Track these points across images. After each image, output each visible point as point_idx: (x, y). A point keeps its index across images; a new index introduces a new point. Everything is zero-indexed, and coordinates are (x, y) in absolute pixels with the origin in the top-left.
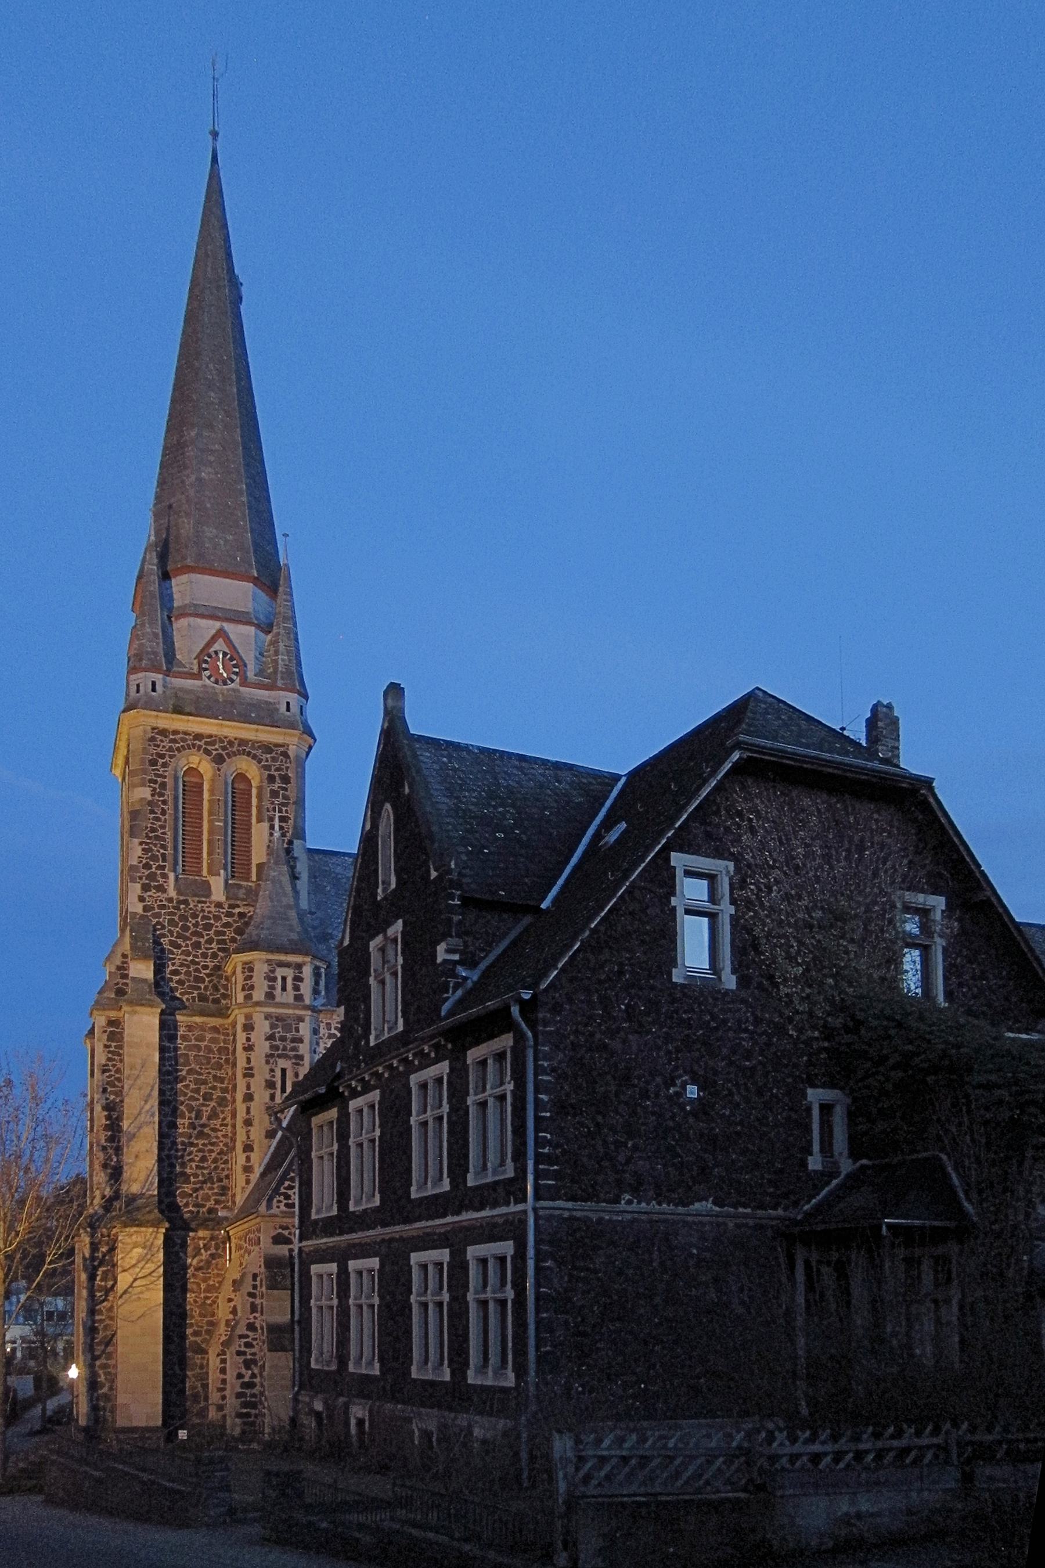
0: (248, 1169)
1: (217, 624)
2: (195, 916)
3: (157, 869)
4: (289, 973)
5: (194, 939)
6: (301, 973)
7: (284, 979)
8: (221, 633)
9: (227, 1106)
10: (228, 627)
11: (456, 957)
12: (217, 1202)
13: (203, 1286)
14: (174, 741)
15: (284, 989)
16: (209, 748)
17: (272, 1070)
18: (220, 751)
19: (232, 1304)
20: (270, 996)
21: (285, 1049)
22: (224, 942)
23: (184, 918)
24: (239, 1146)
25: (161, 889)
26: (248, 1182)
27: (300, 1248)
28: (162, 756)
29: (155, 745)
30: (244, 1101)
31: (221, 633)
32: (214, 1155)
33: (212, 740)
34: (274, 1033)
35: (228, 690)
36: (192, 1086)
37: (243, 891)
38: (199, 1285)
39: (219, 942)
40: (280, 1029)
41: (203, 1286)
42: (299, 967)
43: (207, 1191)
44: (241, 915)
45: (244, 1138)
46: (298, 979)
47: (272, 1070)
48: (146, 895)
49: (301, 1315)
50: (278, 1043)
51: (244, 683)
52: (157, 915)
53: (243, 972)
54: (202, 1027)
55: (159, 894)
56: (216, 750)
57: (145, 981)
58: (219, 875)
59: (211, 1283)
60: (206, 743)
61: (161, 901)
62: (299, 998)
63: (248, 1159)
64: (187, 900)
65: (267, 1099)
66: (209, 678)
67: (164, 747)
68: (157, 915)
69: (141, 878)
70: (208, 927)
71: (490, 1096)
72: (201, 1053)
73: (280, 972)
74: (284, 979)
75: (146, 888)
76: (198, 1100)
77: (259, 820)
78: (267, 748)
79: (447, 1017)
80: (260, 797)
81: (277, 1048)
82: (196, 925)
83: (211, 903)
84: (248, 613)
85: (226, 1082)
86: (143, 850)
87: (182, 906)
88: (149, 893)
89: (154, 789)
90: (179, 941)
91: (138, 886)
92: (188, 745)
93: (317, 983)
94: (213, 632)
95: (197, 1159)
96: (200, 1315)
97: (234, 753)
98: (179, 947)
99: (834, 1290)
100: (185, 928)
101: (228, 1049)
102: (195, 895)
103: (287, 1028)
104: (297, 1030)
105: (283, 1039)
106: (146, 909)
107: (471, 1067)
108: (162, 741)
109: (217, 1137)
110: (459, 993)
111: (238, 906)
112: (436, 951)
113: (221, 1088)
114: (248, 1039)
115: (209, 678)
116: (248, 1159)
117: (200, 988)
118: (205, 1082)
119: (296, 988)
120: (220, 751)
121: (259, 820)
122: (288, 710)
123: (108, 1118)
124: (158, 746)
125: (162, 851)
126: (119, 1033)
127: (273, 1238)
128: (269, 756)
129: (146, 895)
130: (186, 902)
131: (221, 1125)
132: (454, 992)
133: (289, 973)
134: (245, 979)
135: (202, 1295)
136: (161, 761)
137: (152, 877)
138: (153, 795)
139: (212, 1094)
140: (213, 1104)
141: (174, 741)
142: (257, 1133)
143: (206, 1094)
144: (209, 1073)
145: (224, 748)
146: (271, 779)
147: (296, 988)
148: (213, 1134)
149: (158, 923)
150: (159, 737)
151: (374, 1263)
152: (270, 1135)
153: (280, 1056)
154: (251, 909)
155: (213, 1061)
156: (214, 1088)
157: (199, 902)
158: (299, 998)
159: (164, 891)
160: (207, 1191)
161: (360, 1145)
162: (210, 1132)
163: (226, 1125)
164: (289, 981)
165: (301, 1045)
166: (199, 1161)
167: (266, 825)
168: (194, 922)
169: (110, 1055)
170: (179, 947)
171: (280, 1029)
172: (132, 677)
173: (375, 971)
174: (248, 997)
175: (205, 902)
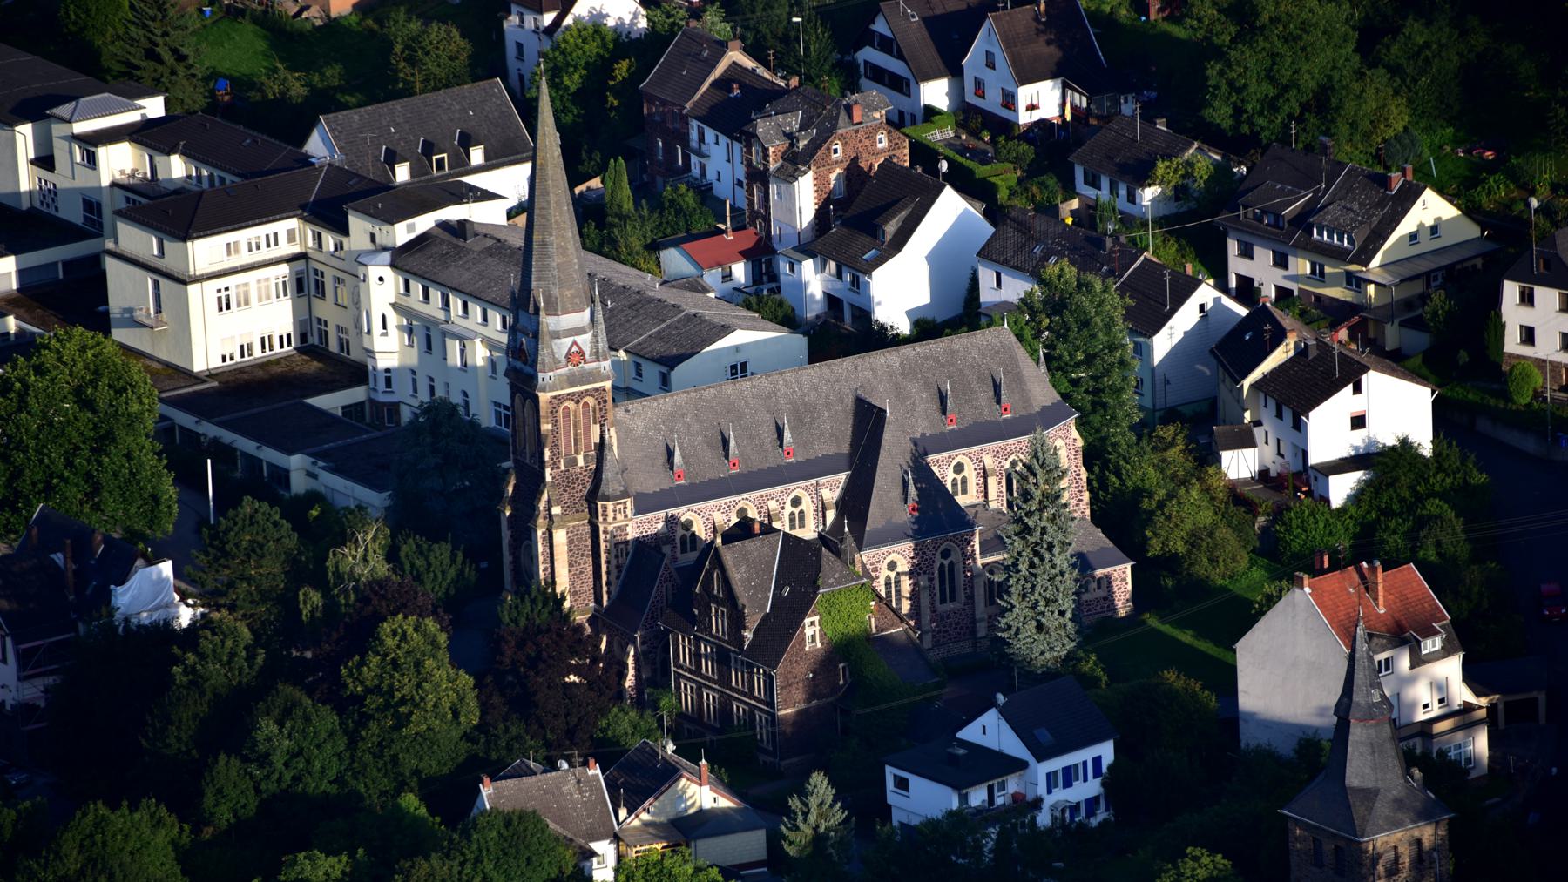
8: (575, 343)
20: (615, 518)
23: (568, 478)
25: (558, 468)
31: (575, 343)
33: (574, 394)
42: (625, 503)
46: (625, 508)
51: (585, 363)
54: (579, 526)
58: (1108, 577)
62: (626, 516)
70: (577, 479)
71: (610, 524)
73: (618, 507)
75: (552, 469)
77: (595, 423)
78: (597, 390)
80: (594, 411)
84: (548, 315)
99: (527, 732)
103: (622, 530)
121: (595, 423)
127: (895, 563)
137: (554, 463)
146: (599, 404)
152: (618, 577)
167: (598, 426)
172: (1105, 594)
174: (605, 519)
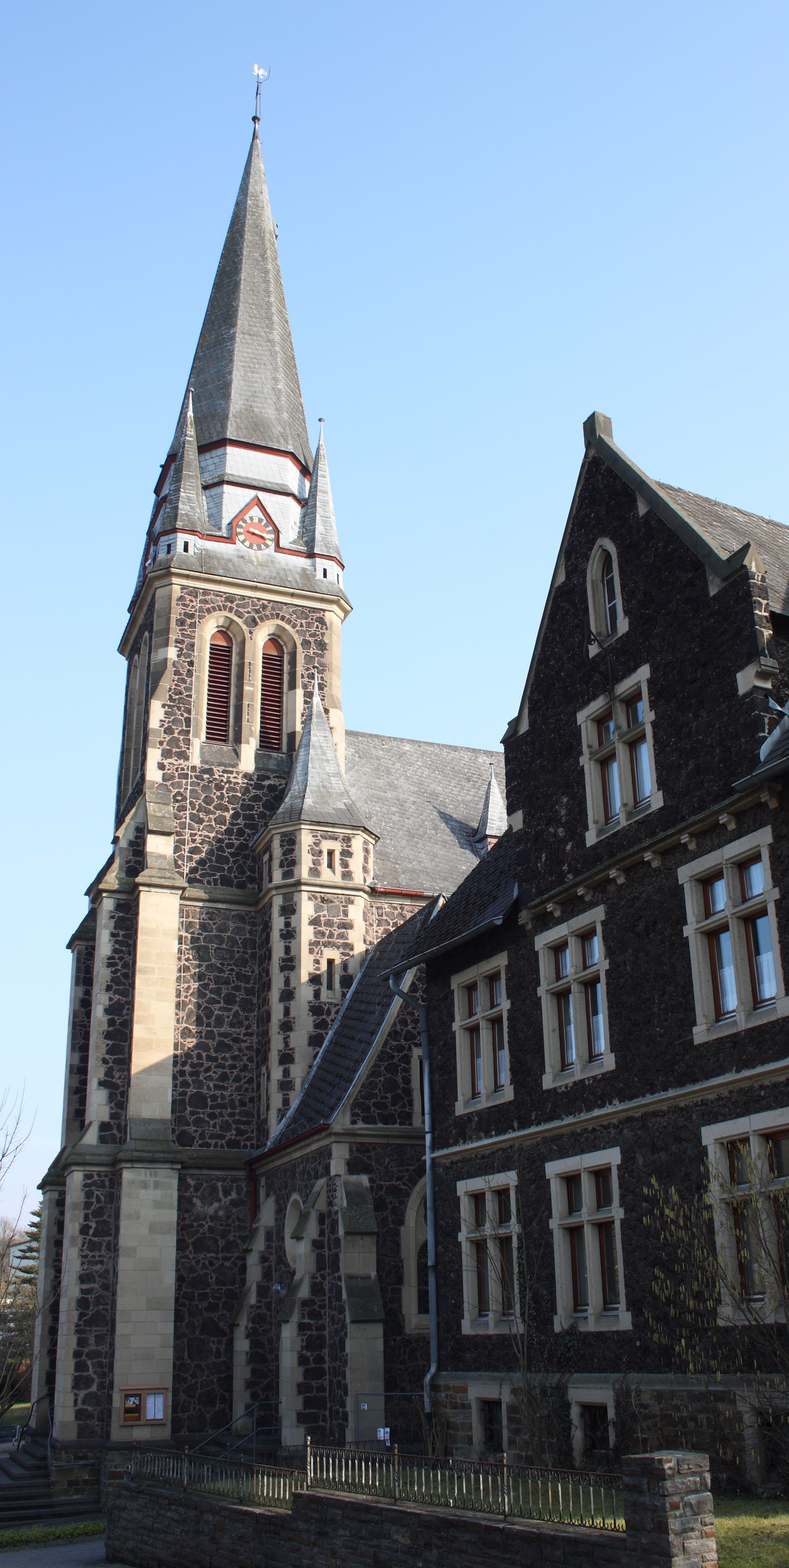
0: (286, 1085)
1: (252, 493)
2: (219, 787)
3: (179, 733)
4: (337, 846)
5: (218, 813)
6: (350, 846)
7: (331, 853)
9: (253, 1011)
10: (262, 495)
11: (768, 685)
12: (240, 1133)
13: (221, 1243)
14: (206, 602)
15: (330, 865)
16: (241, 610)
17: (317, 962)
18: (253, 614)
19: (266, 1264)
21: (331, 935)
22: (251, 817)
24: (274, 1057)
25: (184, 756)
26: (286, 1102)
27: (433, 1160)
28: (192, 616)
29: (184, 605)
30: (281, 1000)
32: (236, 1072)
34: (319, 916)
35: (263, 555)
36: (212, 986)
37: (273, 762)
38: (216, 1241)
39: (246, 817)
40: (325, 912)
41: (221, 1243)
42: (347, 840)
43: (226, 1118)
44: (271, 788)
45: (281, 1046)
46: (347, 854)
47: (317, 962)
48: (166, 762)
49: (437, 1256)
50: (323, 928)
52: (179, 785)
53: (282, 846)
55: (181, 761)
56: (248, 612)
57: (164, 857)
59: (232, 1238)
60: (238, 606)
61: (183, 769)
63: (286, 1073)
64: (212, 769)
65: (311, 997)
66: (243, 542)
67: (193, 607)
68: (179, 785)
69: (161, 743)
72: (224, 946)
73: (326, 846)
74: (331, 853)
75: (166, 754)
76: (219, 1002)
79: (767, 761)
81: (323, 934)
82: (222, 797)
83: (238, 773)
85: (252, 982)
86: (166, 713)
87: (206, 776)
88: (169, 760)
89: (181, 650)
90: (201, 815)
91: (159, 752)
92: (219, 606)
93: (366, 860)
94: (248, 500)
95: (215, 1076)
96: (218, 1282)
97: (266, 616)
98: (201, 821)
100: (208, 800)
101: (254, 942)
102: (220, 765)
104: (346, 914)
105: (329, 923)
106: (165, 778)
107: (687, 888)
108: (191, 601)
109: (240, 1050)
110: (777, 732)
111: (268, 778)
112: (736, 681)
113: (246, 989)
114: (288, 924)
115: (243, 542)
116: (286, 1073)
117: (223, 870)
118: (227, 982)
119: (345, 865)
120: (253, 614)
122: (325, 576)
123: (111, 1023)
124: (187, 606)
125: (186, 715)
126: (128, 919)
128: (303, 621)
129: (166, 762)
130: (210, 772)
131: (245, 1035)
132: (770, 733)
133: (337, 846)
134: (284, 854)
135: (220, 1255)
136: (189, 621)
138: (179, 656)
139: (235, 996)
140: (235, 1008)
141: (206, 602)
142: (299, 1039)
143: (227, 995)
144: (232, 970)
145: (257, 612)
147: (345, 865)
148: (235, 1046)
149: (179, 793)
150: (188, 597)
151: (612, 1157)
152: (315, 1041)
153: (326, 945)
154: (283, 782)
155: (237, 956)
156: (237, 988)
157: (224, 772)
158: (347, 875)
159: (187, 758)
160: (226, 1118)
161: (473, 1031)
162: (231, 1043)
163: (251, 1035)
164: (337, 856)
165: (350, 931)
166: (217, 1080)
168: (218, 793)
169: (117, 946)
170: (201, 821)
171: (325, 912)
173: (589, 747)
175: (232, 772)
